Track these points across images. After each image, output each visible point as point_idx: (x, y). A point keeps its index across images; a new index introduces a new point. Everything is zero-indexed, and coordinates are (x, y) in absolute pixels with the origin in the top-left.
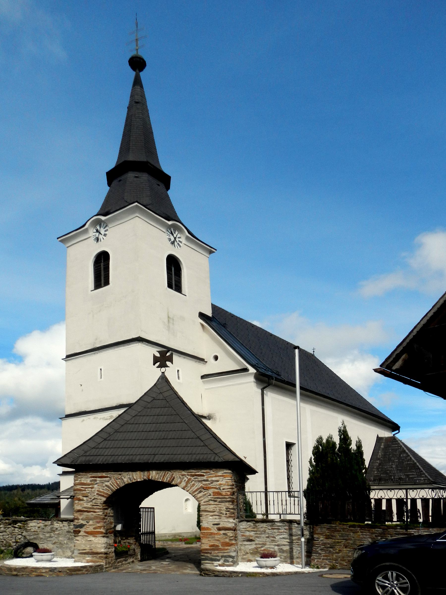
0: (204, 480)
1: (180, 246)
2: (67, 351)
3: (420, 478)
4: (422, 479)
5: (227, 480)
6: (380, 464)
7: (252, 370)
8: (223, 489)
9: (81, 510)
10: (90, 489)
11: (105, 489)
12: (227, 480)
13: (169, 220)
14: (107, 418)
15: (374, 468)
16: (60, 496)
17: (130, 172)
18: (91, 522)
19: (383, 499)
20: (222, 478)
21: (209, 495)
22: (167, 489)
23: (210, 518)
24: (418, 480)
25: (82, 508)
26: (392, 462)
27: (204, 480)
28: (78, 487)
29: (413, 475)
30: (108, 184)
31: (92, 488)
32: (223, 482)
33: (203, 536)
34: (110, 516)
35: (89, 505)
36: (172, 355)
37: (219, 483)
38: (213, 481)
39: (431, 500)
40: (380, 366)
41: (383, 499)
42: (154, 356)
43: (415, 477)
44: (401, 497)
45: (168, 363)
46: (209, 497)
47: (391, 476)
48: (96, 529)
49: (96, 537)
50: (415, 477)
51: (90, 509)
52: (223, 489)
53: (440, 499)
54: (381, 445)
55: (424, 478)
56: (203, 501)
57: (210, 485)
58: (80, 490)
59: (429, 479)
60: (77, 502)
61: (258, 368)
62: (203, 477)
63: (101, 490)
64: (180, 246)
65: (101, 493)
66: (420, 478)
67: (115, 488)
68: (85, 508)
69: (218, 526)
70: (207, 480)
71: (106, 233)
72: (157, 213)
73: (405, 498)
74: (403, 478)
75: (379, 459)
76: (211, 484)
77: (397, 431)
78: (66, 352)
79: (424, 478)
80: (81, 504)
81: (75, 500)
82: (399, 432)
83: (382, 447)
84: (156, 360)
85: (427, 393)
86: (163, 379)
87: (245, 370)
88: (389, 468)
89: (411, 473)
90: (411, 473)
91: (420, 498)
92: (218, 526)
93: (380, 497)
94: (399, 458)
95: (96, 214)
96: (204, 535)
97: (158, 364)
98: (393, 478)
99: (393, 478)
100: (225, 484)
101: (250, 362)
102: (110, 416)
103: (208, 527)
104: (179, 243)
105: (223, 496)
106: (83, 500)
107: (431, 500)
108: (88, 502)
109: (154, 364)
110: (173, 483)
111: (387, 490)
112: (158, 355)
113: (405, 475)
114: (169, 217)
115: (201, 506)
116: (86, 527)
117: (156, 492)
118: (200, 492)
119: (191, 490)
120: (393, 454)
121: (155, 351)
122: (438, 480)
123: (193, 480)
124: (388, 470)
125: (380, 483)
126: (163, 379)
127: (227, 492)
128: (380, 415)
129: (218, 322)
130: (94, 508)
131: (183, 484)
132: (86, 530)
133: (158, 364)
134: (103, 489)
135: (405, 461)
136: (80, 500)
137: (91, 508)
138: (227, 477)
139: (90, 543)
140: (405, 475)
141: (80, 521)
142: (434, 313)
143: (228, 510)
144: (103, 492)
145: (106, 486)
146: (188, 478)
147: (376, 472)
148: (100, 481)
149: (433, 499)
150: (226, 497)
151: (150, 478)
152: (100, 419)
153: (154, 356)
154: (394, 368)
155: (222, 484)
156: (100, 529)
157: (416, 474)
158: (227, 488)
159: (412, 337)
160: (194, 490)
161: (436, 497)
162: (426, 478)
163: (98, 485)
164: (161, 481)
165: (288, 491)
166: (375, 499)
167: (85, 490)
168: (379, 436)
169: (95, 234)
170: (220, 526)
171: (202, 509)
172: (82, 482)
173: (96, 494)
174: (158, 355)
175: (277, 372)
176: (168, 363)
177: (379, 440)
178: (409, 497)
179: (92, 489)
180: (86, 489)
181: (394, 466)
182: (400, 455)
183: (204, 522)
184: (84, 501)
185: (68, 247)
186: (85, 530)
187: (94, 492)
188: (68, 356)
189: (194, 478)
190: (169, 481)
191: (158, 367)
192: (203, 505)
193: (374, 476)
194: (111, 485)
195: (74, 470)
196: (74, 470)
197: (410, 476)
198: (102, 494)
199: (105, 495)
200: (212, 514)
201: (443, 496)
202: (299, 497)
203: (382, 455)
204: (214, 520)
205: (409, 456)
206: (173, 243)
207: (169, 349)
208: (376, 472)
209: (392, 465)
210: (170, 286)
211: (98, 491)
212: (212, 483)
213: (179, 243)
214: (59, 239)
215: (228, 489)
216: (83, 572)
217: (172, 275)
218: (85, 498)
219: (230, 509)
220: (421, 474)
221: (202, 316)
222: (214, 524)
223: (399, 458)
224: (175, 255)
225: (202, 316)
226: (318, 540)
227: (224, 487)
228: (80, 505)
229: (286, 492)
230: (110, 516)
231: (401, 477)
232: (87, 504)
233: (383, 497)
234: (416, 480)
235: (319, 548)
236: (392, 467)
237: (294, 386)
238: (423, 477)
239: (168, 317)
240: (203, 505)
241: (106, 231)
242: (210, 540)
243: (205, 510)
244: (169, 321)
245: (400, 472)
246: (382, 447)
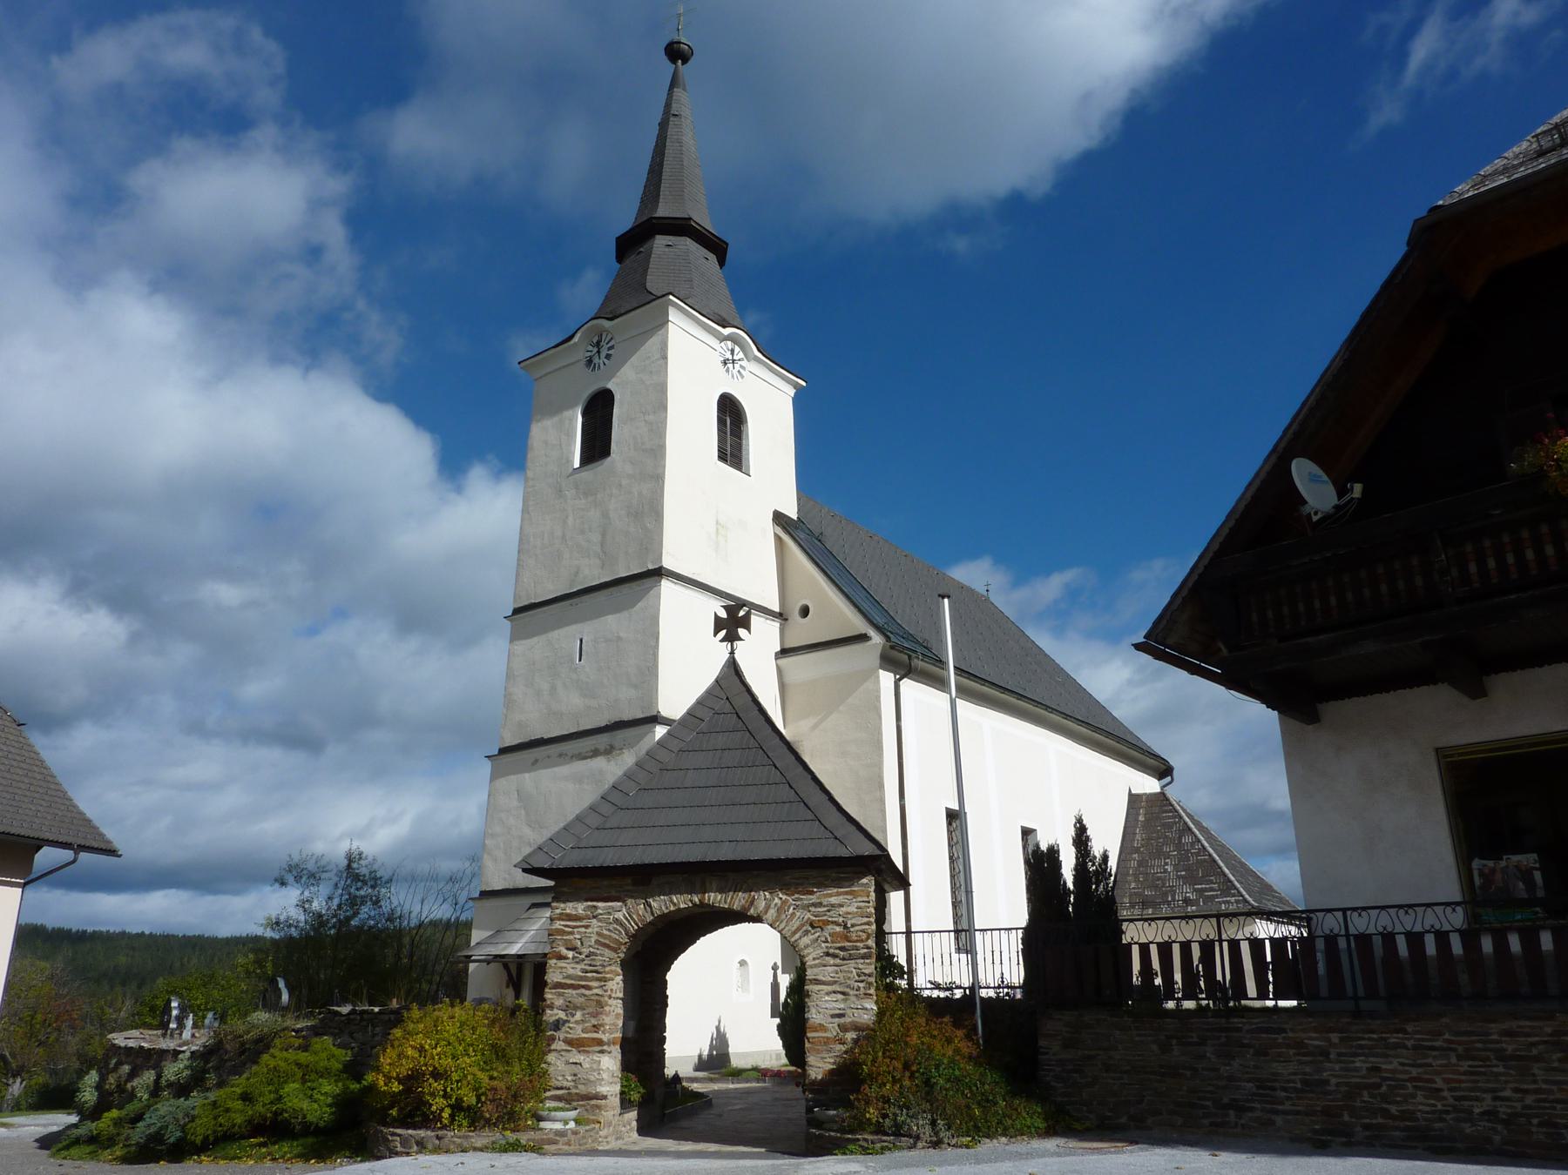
0: (814, 905)
1: (742, 377)
2: (516, 597)
3: (1228, 899)
4: (1233, 899)
5: (860, 902)
6: (1140, 863)
7: (877, 639)
8: (853, 926)
9: (560, 983)
10: (583, 930)
11: (611, 928)
12: (860, 902)
13: (724, 327)
14: (587, 755)
15: (1128, 874)
16: (471, 956)
17: (658, 237)
18: (578, 1016)
19: (1174, 942)
20: (849, 897)
21: (824, 942)
22: (739, 925)
23: (827, 998)
24: (1224, 902)
25: (564, 978)
26: (1165, 859)
27: (814, 905)
28: (558, 925)
29: (1212, 890)
30: (617, 258)
31: (586, 927)
32: (853, 909)
33: (810, 1045)
34: (617, 998)
35: (577, 970)
36: (748, 615)
37: (844, 909)
38: (833, 906)
39: (1267, 942)
40: (1144, 637)
41: (1174, 942)
42: (717, 617)
43: (1217, 896)
44: (1208, 936)
45: (742, 632)
46: (823, 945)
47: (1166, 894)
48: (587, 1033)
49: (588, 1052)
50: (1217, 896)
51: (579, 981)
52: (853, 926)
53: (1285, 939)
54: (1138, 814)
55: (1237, 898)
56: (811, 957)
57: (825, 915)
58: (562, 932)
59: (1245, 901)
60: (554, 961)
61: (889, 634)
62: (811, 897)
63: (605, 932)
64: (742, 377)
65: (605, 939)
66: (1228, 899)
67: (633, 927)
68: (569, 977)
69: (842, 1020)
70: (820, 905)
71: (610, 352)
72: (705, 313)
73: (1217, 938)
74: (1190, 900)
75: (1137, 850)
76: (828, 913)
77: (1169, 779)
78: (515, 601)
79: (1237, 898)
80: (561, 968)
81: (550, 959)
82: (1172, 779)
83: (1141, 818)
84: (719, 624)
85: (1232, 692)
86: (733, 667)
87: (863, 638)
88: (1161, 873)
89: (1207, 886)
90: (1207, 886)
91: (1247, 939)
92: (842, 1020)
93: (1167, 939)
94: (1179, 846)
95: (593, 315)
96: (812, 1043)
97: (723, 633)
98: (1170, 899)
99: (1170, 899)
100: (857, 912)
101: (871, 617)
102: (592, 751)
103: (822, 1022)
104: (741, 371)
105: (851, 942)
106: (566, 958)
107: (1267, 942)
108: (577, 963)
109: (715, 634)
110: (752, 912)
111: (1179, 921)
112: (723, 614)
113: (1195, 890)
114: (724, 320)
115: (808, 970)
116: (569, 1027)
117: (702, 938)
118: (807, 932)
119: (787, 928)
120: (1166, 836)
121: (718, 608)
122: (1266, 902)
123: (791, 904)
124: (1159, 879)
125: (1144, 912)
126: (733, 667)
127: (861, 933)
128: (1128, 738)
129: (808, 532)
130: (586, 979)
131: (772, 913)
132: (569, 1036)
133: (723, 633)
134: (609, 930)
135: (1191, 853)
136: (561, 957)
137: (581, 978)
138: (861, 896)
139: (575, 1069)
140: (1195, 890)
141: (555, 1011)
142: (1230, 529)
143: (863, 978)
144: (610, 936)
145: (617, 921)
146: (781, 899)
147: (1133, 885)
148: (604, 908)
149: (1272, 939)
150: (858, 944)
151: (706, 901)
152: (572, 757)
153: (717, 617)
154: (1170, 641)
155: (849, 913)
156: (596, 1032)
157: (1219, 886)
158: (859, 923)
159: (1197, 577)
160: (793, 929)
161: (1276, 936)
162: (1241, 898)
163: (600, 921)
164: (726, 906)
165: (953, 929)
166: (1158, 944)
167: (572, 933)
168: (1133, 792)
169: (590, 348)
170: (847, 1020)
171: (810, 977)
172: (568, 911)
173: (593, 940)
174: (723, 614)
175: (925, 640)
176: (742, 632)
177: (1134, 799)
178: (1224, 936)
179: (588, 931)
180: (576, 930)
181: (1169, 868)
182: (1180, 838)
183: (813, 1010)
184: (567, 961)
185: (536, 380)
186: (566, 1035)
187: (590, 937)
188: (517, 611)
189: (793, 900)
190: (743, 906)
191: (722, 641)
192: (811, 967)
193: (1130, 896)
194: (627, 919)
195: (551, 883)
196: (551, 883)
197: (1206, 894)
198: (607, 942)
199: (612, 945)
200: (830, 988)
201: (1290, 933)
202: (969, 949)
203: (1143, 840)
204: (834, 1005)
205: (1199, 841)
206: (725, 363)
207: (742, 603)
208: (1133, 885)
209: (1166, 864)
210: (722, 456)
211: (599, 934)
212: (829, 911)
213: (741, 371)
214: (522, 364)
215: (861, 924)
216: (560, 1146)
217: (726, 433)
218: (570, 954)
219: (865, 975)
220: (1229, 889)
221: (779, 518)
222: (833, 1016)
223: (1179, 846)
224: (735, 395)
225: (779, 518)
226: (1047, 1053)
227: (853, 921)
228: (560, 970)
229: (949, 931)
230: (617, 998)
231: (1188, 895)
232: (573, 968)
233: (1173, 938)
234: (1220, 903)
235: (1051, 1074)
236: (1165, 871)
237: (941, 663)
238: (1234, 896)
239: (717, 523)
240: (811, 967)
241: (609, 349)
242: (826, 1058)
243: (815, 980)
244: (717, 529)
245: (1184, 883)
246: (1141, 818)
